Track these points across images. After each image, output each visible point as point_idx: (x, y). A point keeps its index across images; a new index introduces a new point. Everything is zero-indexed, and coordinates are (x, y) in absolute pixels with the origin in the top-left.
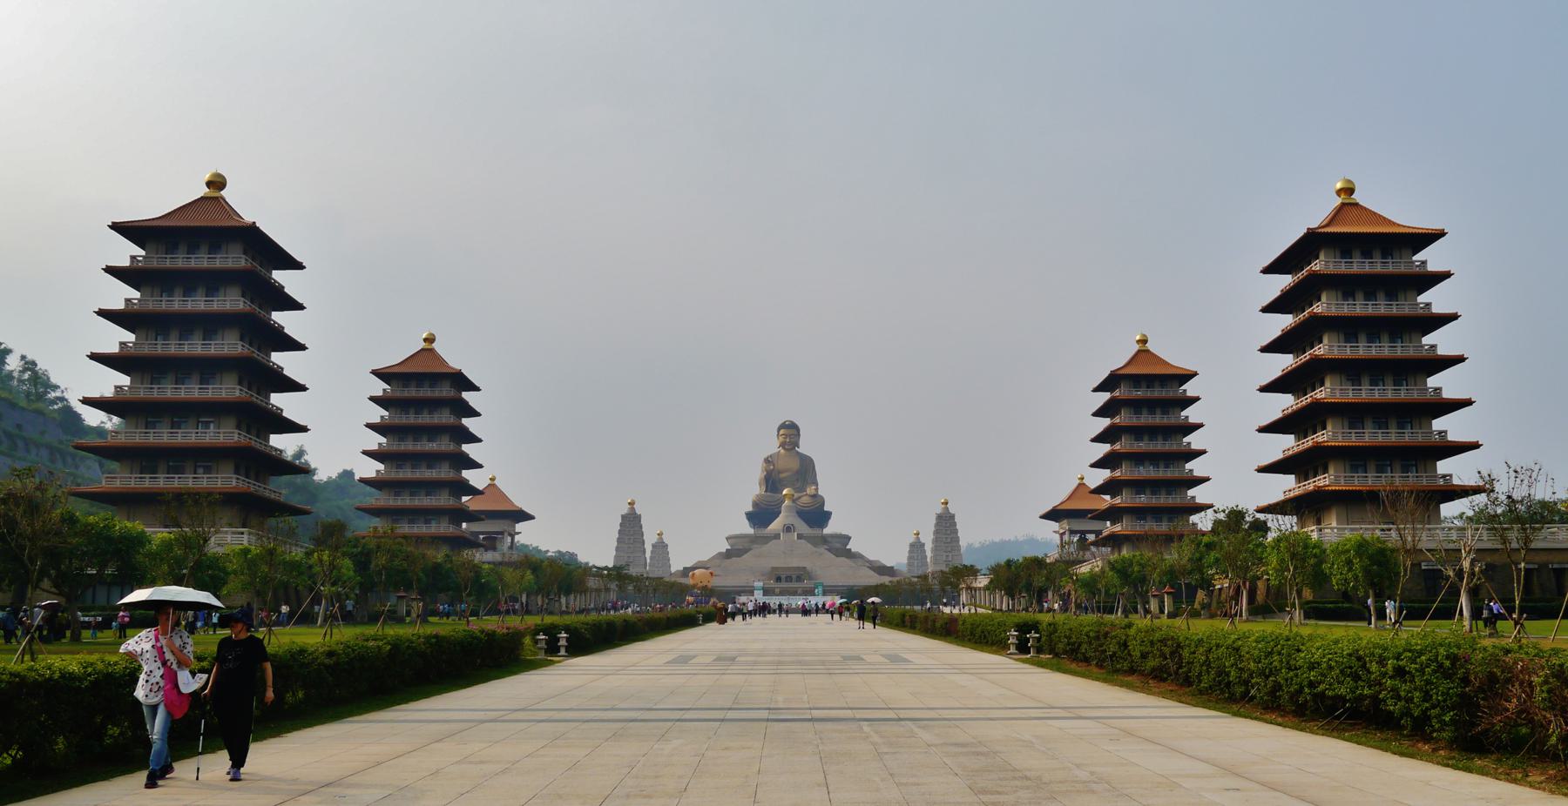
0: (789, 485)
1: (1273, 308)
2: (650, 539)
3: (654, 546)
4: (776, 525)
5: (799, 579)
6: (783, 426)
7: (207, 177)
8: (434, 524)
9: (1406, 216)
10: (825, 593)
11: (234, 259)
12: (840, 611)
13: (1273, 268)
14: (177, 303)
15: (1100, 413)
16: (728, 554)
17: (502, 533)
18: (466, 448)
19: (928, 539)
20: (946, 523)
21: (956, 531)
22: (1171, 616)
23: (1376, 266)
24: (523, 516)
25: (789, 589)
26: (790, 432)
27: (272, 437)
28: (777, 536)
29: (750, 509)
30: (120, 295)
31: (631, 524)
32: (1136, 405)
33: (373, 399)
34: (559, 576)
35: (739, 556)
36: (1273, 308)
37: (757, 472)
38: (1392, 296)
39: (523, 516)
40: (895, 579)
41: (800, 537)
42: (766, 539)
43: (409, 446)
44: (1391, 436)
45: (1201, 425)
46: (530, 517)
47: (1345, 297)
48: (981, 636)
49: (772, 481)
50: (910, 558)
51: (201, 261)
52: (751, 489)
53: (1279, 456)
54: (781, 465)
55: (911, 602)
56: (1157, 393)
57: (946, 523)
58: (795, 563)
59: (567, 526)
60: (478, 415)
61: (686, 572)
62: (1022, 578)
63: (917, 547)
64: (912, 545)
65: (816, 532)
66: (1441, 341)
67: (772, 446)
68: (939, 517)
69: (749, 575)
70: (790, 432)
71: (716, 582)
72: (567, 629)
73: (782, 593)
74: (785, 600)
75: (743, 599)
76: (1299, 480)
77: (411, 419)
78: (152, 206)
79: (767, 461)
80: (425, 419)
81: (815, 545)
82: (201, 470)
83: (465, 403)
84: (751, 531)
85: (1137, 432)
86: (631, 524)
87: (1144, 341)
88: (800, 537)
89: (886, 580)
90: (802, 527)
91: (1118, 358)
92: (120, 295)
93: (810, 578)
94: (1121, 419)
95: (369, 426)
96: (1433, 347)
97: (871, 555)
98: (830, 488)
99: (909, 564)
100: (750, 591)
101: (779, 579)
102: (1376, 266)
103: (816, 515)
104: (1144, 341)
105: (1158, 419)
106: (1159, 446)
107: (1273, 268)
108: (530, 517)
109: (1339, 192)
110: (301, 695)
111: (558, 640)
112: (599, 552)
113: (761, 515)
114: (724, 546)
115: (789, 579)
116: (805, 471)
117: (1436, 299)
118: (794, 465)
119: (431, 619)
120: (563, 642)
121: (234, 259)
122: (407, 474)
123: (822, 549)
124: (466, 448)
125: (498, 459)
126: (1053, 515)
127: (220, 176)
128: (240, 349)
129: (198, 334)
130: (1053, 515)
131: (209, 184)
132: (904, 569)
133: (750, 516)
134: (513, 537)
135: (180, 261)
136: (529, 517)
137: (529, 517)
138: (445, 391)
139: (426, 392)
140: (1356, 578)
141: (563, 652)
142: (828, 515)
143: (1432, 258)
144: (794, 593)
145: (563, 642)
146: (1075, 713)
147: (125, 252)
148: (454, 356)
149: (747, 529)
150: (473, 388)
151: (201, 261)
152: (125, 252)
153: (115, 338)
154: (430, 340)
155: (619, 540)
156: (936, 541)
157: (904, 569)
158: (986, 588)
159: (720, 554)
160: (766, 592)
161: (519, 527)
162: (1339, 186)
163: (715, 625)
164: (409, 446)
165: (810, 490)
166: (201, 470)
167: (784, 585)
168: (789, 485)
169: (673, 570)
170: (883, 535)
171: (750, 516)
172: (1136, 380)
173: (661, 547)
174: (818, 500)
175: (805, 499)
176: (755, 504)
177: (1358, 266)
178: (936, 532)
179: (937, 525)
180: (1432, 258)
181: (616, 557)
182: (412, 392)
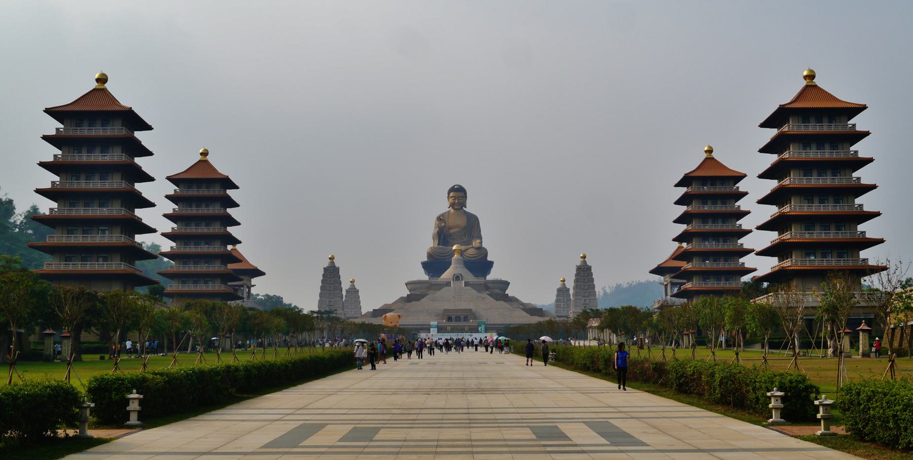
0: (458, 235)
1: (765, 150)
2: (345, 286)
3: (347, 291)
4: (447, 275)
5: (466, 319)
6: (453, 189)
7: (97, 76)
8: (210, 284)
9: (846, 95)
10: (486, 331)
11: (116, 130)
12: (499, 346)
13: (766, 124)
14: (84, 157)
15: (679, 202)
16: (408, 299)
17: (242, 286)
18: (139, 186)
19: (570, 284)
20: (584, 273)
21: (593, 280)
22: (866, 355)
23: (825, 128)
24: (258, 273)
25: (458, 332)
26: (458, 194)
27: (136, 236)
28: (448, 284)
29: (426, 259)
30: (50, 153)
31: (331, 274)
32: (703, 198)
33: (46, 138)
34: (288, 320)
35: (418, 300)
36: (765, 150)
37: (430, 229)
38: (834, 146)
39: (258, 273)
40: (547, 319)
41: (467, 284)
42: (440, 286)
43: (193, 229)
44: (832, 235)
45: (748, 213)
46: (263, 274)
47: (804, 148)
48: (592, 365)
49: (443, 235)
50: (557, 301)
51: (98, 131)
52: (426, 242)
53: (768, 244)
54: (451, 222)
55: (532, 340)
56: (719, 189)
57: (584, 273)
58: (463, 306)
59: (285, 279)
60: (237, 205)
61: (377, 313)
62: (625, 320)
63: (562, 291)
64: (559, 290)
65: (480, 280)
66: (864, 175)
67: (443, 206)
68: (579, 269)
69: (426, 317)
70: (458, 194)
71: (403, 322)
72: (139, 384)
73: (453, 330)
74: (467, 337)
75: (423, 335)
76: (780, 261)
77: (193, 211)
78: (65, 97)
79: (440, 219)
80: (204, 211)
81: (479, 291)
82: (101, 259)
83: (138, 143)
84: (426, 278)
85: (704, 217)
86: (331, 274)
87: (710, 151)
88: (467, 284)
89: (535, 319)
90: (469, 277)
91: (691, 163)
92: (50, 153)
93: (475, 318)
94: (695, 207)
95: (43, 165)
96: (859, 179)
97: (525, 300)
98: (492, 240)
99: (557, 306)
100: (427, 329)
101: (450, 319)
102: (825, 128)
103: (480, 265)
104: (710, 151)
105: (719, 208)
106: (719, 227)
107: (766, 124)
108: (263, 274)
109: (706, 152)
110: (134, 395)
111: (127, 402)
112: (307, 300)
113: (435, 264)
114: (405, 292)
115: (458, 319)
116: (472, 226)
117: (861, 149)
118: (462, 222)
119: (85, 357)
120: (134, 406)
121: (116, 130)
122: (192, 249)
123: (485, 295)
124: (139, 186)
125: (251, 239)
126: (659, 270)
127: (103, 75)
128: (123, 186)
129: (97, 176)
130: (659, 270)
131: (98, 80)
132: (553, 312)
133: (425, 265)
134: (249, 288)
135: (85, 131)
136: (262, 274)
137: (262, 274)
138: (216, 191)
139: (204, 192)
140: (756, 327)
141: (134, 419)
142: (490, 264)
143: (859, 122)
144: (462, 330)
145: (134, 406)
146: (585, 392)
147: (52, 126)
148: (222, 166)
149: (423, 276)
150: (147, 127)
151: (98, 131)
152: (52, 126)
153: (48, 179)
154: (205, 154)
155: (322, 288)
156: (576, 288)
157: (553, 312)
158: (598, 328)
159: (402, 298)
160: (441, 329)
161: (254, 281)
162: (805, 73)
163: (391, 360)
164: (193, 229)
165: (476, 243)
166: (101, 259)
167: (454, 324)
168: (458, 235)
169: (364, 312)
170: (535, 284)
171: (425, 265)
172: (703, 180)
173: (353, 292)
174: (482, 252)
175: (471, 251)
176: (430, 255)
177: (813, 128)
178: (576, 281)
179: (577, 275)
180: (859, 122)
181: (320, 302)
182: (193, 192)
